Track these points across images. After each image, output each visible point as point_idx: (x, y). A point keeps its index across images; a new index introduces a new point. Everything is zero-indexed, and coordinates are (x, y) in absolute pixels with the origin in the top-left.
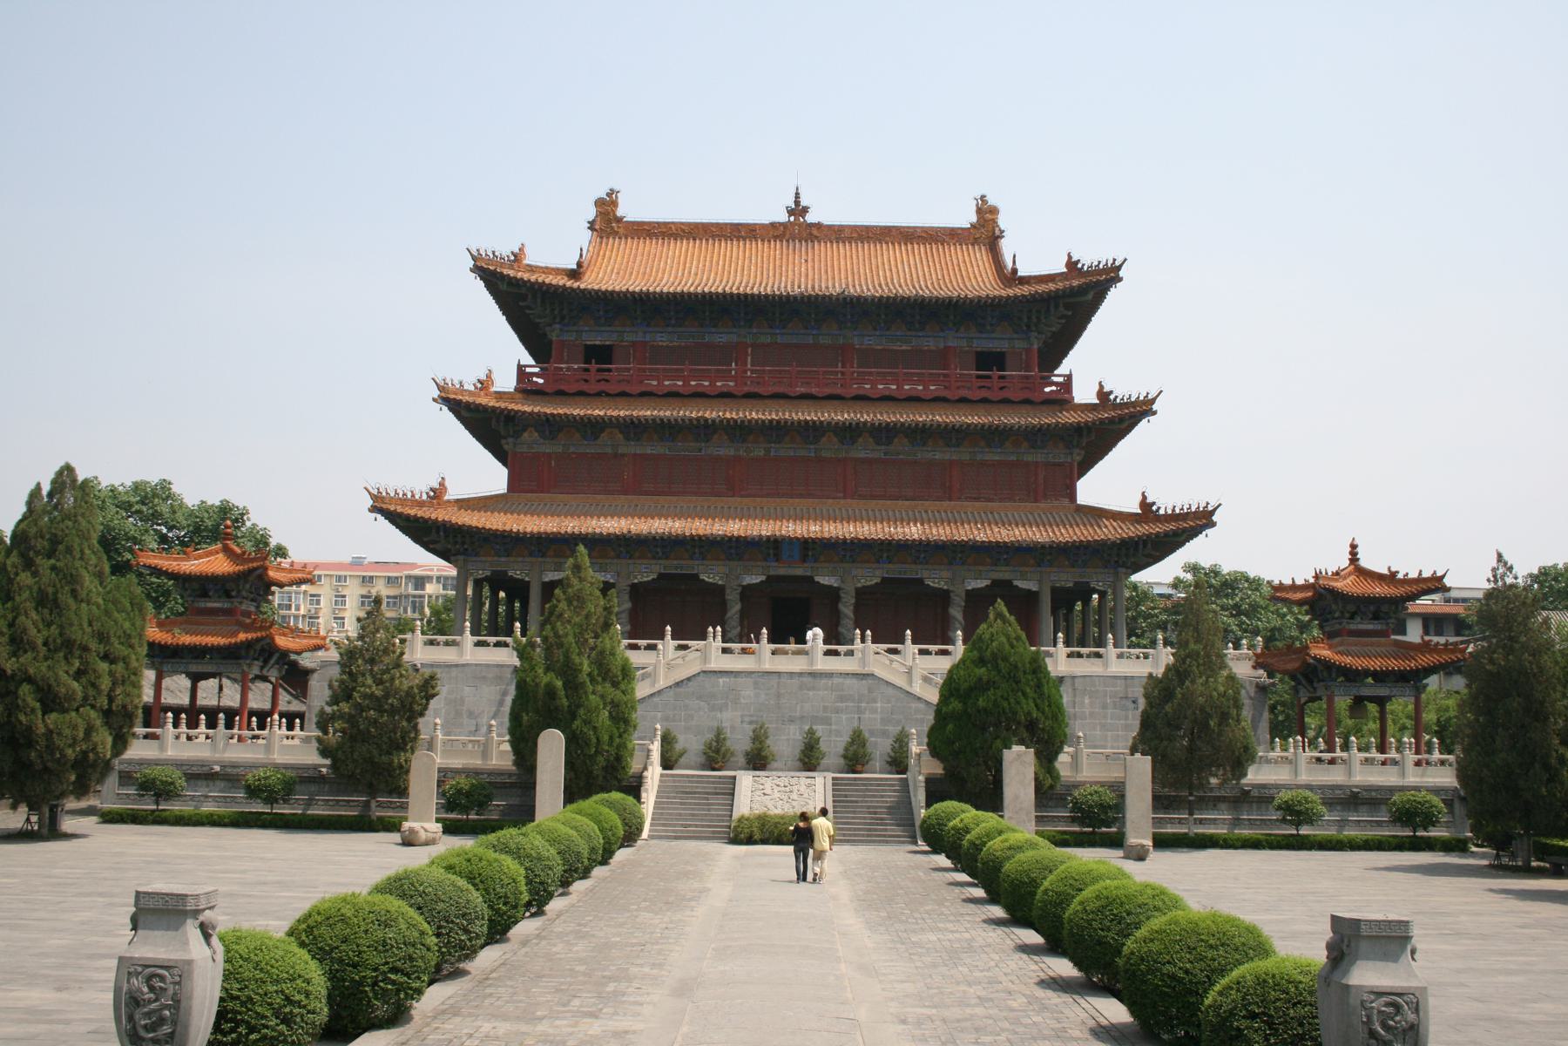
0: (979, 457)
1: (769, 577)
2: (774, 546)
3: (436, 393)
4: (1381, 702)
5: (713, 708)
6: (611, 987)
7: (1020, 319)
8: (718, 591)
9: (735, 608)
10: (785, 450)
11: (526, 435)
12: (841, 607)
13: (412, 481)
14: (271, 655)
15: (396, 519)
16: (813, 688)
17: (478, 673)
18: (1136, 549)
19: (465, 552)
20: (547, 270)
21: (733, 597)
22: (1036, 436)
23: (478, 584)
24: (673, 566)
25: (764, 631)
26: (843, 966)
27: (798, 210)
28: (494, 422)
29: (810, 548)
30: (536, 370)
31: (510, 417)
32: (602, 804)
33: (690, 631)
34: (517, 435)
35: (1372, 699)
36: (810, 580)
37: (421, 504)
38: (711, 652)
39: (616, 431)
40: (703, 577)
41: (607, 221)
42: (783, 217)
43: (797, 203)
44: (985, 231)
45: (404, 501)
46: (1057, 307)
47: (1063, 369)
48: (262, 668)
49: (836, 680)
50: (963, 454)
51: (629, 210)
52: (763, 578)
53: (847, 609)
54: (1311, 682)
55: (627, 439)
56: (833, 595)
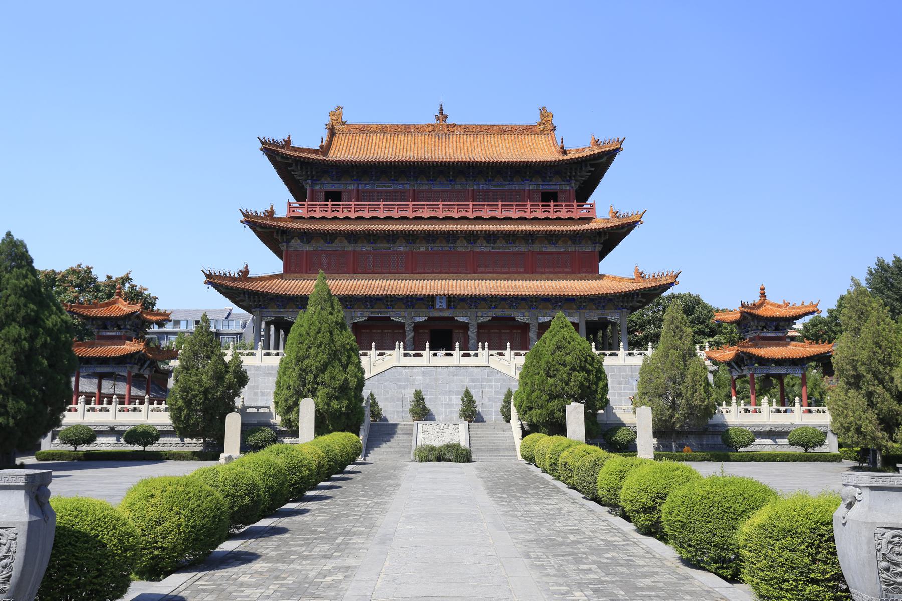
0: (544, 250)
1: (429, 318)
2: (429, 301)
3: (242, 218)
4: (780, 377)
6: (339, 540)
7: (566, 173)
8: (402, 326)
9: (410, 335)
10: (437, 248)
12: (469, 333)
13: (229, 266)
14: (145, 362)
15: (219, 288)
17: (267, 371)
18: (633, 298)
19: (260, 306)
20: (302, 150)
21: (409, 328)
23: (268, 324)
24: (376, 312)
25: (428, 343)
26: (484, 525)
29: (454, 301)
31: (284, 232)
32: (339, 440)
33: (385, 345)
34: (288, 242)
35: (774, 376)
36: (452, 318)
37: (233, 279)
38: (396, 357)
40: (392, 318)
41: (444, 126)
42: (433, 121)
43: (442, 113)
44: (546, 125)
45: (224, 278)
46: (586, 166)
47: (590, 200)
48: (140, 369)
50: (536, 248)
51: (351, 117)
53: (472, 333)
54: (739, 367)
55: (349, 242)
56: (465, 326)
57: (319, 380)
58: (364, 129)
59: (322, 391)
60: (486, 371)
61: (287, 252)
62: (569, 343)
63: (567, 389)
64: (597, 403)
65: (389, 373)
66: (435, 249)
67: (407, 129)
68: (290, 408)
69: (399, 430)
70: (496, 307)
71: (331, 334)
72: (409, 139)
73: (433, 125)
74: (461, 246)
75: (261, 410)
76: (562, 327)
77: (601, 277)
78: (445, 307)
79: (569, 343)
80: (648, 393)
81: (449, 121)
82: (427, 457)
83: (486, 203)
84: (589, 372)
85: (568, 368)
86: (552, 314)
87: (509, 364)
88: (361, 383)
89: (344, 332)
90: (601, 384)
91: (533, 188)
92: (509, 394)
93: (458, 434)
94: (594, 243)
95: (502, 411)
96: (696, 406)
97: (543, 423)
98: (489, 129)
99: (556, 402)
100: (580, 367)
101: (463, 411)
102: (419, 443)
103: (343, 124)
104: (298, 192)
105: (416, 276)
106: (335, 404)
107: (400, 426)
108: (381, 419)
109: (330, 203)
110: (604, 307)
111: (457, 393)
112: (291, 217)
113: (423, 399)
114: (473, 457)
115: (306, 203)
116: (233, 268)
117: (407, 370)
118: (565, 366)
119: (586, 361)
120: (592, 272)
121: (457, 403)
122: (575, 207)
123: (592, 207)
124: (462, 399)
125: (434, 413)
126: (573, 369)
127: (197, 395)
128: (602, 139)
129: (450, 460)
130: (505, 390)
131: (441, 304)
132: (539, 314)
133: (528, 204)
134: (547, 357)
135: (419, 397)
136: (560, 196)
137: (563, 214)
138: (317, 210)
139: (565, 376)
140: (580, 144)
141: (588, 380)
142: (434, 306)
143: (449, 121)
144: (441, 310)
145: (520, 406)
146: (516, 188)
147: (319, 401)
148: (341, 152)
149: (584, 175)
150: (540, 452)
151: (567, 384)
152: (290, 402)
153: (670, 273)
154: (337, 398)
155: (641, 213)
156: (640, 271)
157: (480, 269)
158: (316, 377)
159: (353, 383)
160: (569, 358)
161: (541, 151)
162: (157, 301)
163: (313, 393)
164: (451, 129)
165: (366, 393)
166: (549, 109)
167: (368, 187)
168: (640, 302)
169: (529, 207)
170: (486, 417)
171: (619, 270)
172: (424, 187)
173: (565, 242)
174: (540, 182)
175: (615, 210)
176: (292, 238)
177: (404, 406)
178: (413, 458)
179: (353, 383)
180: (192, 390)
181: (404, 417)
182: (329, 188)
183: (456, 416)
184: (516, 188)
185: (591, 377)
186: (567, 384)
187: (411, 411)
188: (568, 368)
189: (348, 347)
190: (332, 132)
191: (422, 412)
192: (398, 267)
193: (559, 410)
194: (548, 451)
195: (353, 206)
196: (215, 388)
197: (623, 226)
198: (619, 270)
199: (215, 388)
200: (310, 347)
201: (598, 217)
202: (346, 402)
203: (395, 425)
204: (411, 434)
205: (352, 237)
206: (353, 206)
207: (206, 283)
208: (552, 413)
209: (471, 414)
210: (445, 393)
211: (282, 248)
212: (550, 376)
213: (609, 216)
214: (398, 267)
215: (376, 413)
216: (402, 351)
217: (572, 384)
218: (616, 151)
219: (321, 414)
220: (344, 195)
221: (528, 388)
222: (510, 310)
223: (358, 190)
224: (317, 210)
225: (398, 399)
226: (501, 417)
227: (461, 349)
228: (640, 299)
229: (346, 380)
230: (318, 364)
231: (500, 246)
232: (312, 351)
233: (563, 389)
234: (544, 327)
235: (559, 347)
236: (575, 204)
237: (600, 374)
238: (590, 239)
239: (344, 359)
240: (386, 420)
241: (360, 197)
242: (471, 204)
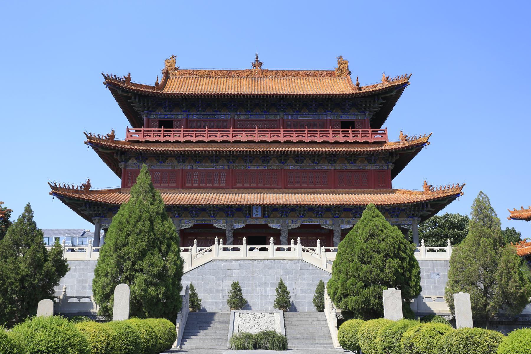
0: (345, 168)
1: (247, 225)
2: (246, 210)
3: (86, 140)
5: (218, 279)
10: (253, 166)
11: (130, 161)
12: (281, 238)
15: (62, 198)
16: (271, 268)
18: (423, 208)
19: (99, 215)
20: (141, 86)
22: (371, 157)
25: (245, 238)
27: (258, 63)
28: (115, 155)
29: (268, 210)
30: (134, 131)
34: (126, 161)
37: (77, 191)
38: (217, 251)
39: (173, 158)
40: (215, 225)
41: (258, 70)
42: (250, 67)
44: (343, 70)
46: (378, 99)
47: (383, 127)
49: (283, 263)
50: (337, 166)
51: (182, 64)
52: (244, 225)
55: (179, 162)
57: (136, 267)
58: (193, 74)
59: (140, 278)
60: (299, 264)
61: (125, 169)
62: (382, 231)
63: (382, 276)
64: (411, 290)
65: (207, 268)
66: (252, 168)
67: (228, 74)
68: (106, 296)
69: (216, 317)
70: (304, 216)
71: (152, 224)
72: (230, 81)
73: (250, 70)
74: (274, 165)
75: (82, 301)
76: (374, 217)
77: (394, 191)
78: (260, 215)
79: (382, 231)
80: (458, 281)
81: (263, 67)
82: (243, 344)
83: (294, 130)
84: (402, 259)
85: (382, 254)
86: (353, 222)
87: (321, 260)
88: (179, 274)
89: (165, 222)
90: (414, 271)
91: (334, 117)
92: (321, 286)
93: (275, 322)
94: (387, 162)
95: (314, 301)
96: (512, 294)
97: (359, 310)
98: (296, 74)
99: (372, 288)
100: (394, 254)
101: (278, 302)
102: (236, 331)
103: (177, 69)
104: (136, 120)
105: (235, 190)
106: (152, 291)
107: (217, 315)
108: (199, 309)
109: (162, 129)
110: (398, 216)
111: (272, 285)
112: (130, 141)
113: (240, 290)
114: (289, 345)
115: (142, 129)
116: (75, 181)
117: (225, 263)
118: (379, 253)
119: (399, 248)
120: (387, 187)
121: (272, 295)
122: (370, 132)
123: (384, 134)
124: (277, 291)
125: (250, 304)
126: (386, 256)
127: (13, 283)
128: (392, 76)
129: (266, 348)
130: (317, 283)
131: (257, 213)
132: (341, 222)
133: (331, 130)
134: (361, 244)
135: (236, 289)
136: (356, 124)
137: (360, 138)
138: (152, 135)
139: (379, 262)
140: (371, 80)
141: (403, 268)
142: (250, 215)
143: (263, 67)
144: (257, 219)
145: (335, 294)
146: (320, 117)
147: (136, 288)
148: (175, 87)
149: (377, 107)
150: (366, 335)
151: (382, 271)
152: (108, 289)
153: (456, 185)
154: (156, 285)
155: (427, 135)
156: (429, 184)
157: (290, 185)
158: (133, 264)
159: (172, 270)
160: (382, 245)
161: (340, 87)
162: (12, 213)
163: (129, 280)
164: (265, 74)
165: (185, 282)
166: (345, 58)
167: (196, 117)
168: (429, 211)
169: (331, 133)
170: (299, 307)
171: (409, 184)
172: (242, 117)
173: (362, 162)
174: (340, 113)
175: (405, 134)
176: (130, 158)
177: (222, 297)
178: (229, 345)
179: (172, 270)
180: (8, 278)
181: (222, 308)
182: (163, 117)
183: (271, 307)
184: (320, 117)
185: (405, 264)
186: (382, 271)
187: (229, 302)
188: (382, 254)
189: (168, 236)
190: (167, 75)
191: (239, 302)
192: (220, 183)
193: (375, 297)
194: (380, 332)
195: (182, 132)
196: (33, 276)
197: (412, 147)
198: (409, 184)
199: (33, 276)
200: (129, 235)
201: (390, 141)
202: (163, 289)
203: (213, 314)
204: (228, 323)
205: (181, 157)
206: (182, 132)
207: (51, 194)
208: (367, 300)
209: (285, 303)
210: (260, 285)
211: (121, 167)
212: (365, 263)
213: (400, 140)
214: (220, 183)
215: (195, 302)
216: (221, 246)
217: (387, 270)
218: (405, 85)
219: (138, 302)
220: (175, 124)
221: (342, 276)
222: (315, 219)
223: (187, 120)
224: (152, 135)
225: (217, 291)
226: (314, 308)
227: (275, 244)
228: (429, 208)
229: (164, 267)
230: (136, 251)
231: (307, 165)
232: (131, 239)
233: (378, 275)
234: (344, 233)
235: (372, 235)
236: (370, 130)
237: (413, 264)
238: (383, 159)
239: (163, 248)
240: (204, 310)
241: (188, 124)
242: (282, 130)
